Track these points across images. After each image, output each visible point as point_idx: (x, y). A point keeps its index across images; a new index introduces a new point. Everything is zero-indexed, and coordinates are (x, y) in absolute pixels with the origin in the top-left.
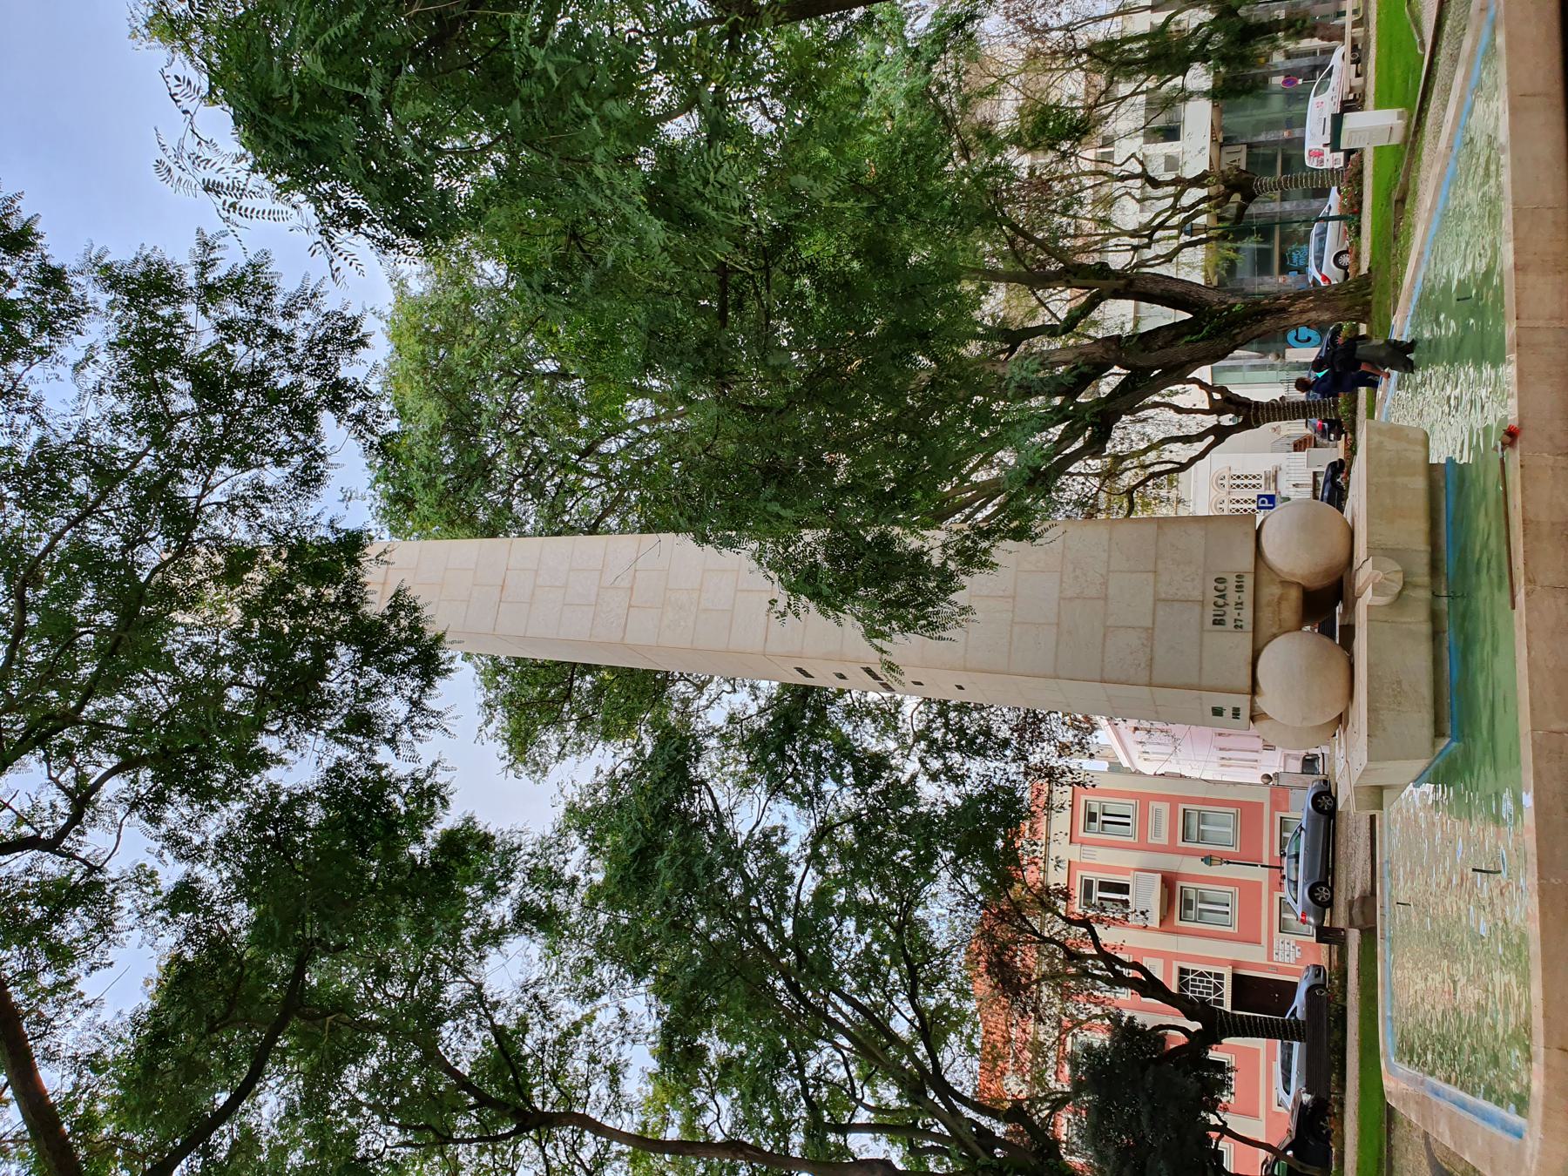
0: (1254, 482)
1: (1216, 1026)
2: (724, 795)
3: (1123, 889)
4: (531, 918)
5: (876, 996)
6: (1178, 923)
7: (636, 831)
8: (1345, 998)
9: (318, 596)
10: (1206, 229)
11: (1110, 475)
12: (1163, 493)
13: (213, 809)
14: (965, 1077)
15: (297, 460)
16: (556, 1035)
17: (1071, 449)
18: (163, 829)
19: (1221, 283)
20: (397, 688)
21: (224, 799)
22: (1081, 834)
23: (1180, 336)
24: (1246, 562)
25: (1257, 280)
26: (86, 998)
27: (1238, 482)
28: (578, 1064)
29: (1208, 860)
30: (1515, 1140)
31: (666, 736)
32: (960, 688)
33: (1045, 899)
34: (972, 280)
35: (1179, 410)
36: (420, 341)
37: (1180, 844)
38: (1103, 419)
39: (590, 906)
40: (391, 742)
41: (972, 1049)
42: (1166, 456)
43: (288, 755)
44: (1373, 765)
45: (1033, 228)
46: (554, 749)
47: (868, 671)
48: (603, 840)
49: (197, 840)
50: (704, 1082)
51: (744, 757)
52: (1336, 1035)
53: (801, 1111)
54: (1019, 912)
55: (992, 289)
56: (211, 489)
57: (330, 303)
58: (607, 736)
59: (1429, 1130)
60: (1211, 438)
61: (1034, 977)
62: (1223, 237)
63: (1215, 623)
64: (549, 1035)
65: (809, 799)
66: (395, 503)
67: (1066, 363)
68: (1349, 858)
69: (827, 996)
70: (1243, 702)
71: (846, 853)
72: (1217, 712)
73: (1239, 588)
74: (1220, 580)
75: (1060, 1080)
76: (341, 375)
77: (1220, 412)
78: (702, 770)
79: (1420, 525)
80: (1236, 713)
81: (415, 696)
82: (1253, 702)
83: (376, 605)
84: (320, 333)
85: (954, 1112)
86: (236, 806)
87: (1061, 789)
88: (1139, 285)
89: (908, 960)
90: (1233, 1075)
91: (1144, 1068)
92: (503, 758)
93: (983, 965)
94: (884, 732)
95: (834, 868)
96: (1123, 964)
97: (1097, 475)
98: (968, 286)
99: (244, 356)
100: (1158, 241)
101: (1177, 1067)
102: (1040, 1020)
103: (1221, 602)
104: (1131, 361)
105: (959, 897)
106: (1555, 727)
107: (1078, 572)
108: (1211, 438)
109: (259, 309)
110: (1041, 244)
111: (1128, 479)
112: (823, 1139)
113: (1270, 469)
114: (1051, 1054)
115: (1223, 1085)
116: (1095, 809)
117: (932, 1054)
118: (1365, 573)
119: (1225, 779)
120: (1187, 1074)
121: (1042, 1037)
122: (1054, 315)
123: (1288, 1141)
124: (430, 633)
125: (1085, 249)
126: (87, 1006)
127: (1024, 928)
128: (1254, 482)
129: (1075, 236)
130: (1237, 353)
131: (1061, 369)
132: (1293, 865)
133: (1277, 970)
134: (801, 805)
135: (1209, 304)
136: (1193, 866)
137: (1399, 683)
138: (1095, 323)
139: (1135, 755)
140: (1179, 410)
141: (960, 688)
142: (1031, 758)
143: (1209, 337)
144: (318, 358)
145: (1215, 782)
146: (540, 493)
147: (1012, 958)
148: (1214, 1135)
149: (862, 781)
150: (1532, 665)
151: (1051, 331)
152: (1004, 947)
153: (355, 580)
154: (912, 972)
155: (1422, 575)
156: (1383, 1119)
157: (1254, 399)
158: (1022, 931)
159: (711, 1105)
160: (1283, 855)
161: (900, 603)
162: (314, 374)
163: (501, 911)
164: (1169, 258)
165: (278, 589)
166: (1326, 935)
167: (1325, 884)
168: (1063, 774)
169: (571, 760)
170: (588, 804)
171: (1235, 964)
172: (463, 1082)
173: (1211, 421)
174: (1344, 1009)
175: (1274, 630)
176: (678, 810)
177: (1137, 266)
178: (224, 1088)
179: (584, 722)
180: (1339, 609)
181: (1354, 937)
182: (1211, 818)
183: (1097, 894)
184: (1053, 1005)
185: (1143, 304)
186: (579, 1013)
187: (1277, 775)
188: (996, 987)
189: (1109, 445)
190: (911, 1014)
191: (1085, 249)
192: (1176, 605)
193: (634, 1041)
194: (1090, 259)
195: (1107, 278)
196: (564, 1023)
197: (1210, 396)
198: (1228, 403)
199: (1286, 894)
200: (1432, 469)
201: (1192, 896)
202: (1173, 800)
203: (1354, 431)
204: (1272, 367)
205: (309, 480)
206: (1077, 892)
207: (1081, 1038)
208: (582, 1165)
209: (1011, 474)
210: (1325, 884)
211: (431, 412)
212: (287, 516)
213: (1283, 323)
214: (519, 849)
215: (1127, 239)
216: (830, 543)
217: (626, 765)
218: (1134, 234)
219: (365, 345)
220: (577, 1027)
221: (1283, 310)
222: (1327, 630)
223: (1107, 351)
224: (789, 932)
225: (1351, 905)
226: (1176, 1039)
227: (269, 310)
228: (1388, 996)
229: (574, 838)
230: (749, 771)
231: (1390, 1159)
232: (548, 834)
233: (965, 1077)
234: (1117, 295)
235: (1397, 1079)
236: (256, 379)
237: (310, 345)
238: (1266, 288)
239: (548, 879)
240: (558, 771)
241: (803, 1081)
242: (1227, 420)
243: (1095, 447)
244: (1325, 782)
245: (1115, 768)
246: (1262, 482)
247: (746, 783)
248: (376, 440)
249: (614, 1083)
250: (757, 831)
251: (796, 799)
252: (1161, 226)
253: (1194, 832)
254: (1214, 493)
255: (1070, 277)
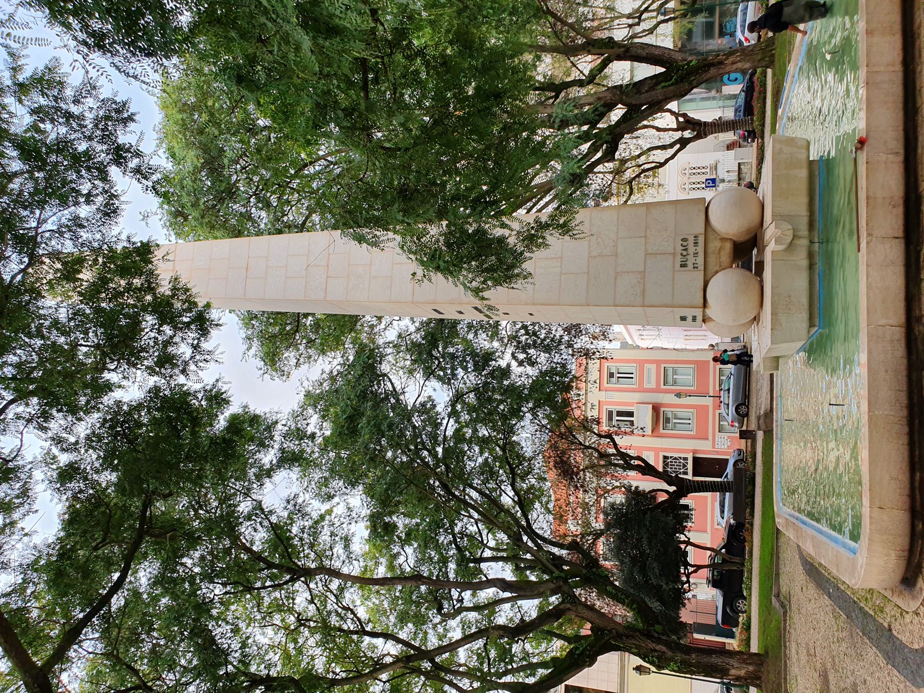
0: (703, 171)
1: (685, 488)
2: (398, 379)
3: (631, 414)
4: (288, 459)
5: (492, 485)
6: (662, 431)
7: (347, 405)
8: (754, 468)
9: (130, 284)
10: (674, 11)
11: (618, 172)
12: (650, 180)
13: (80, 419)
14: (545, 526)
15: (100, 200)
16: (310, 522)
17: (593, 160)
18: (50, 434)
19: (683, 46)
20: (183, 339)
21: (87, 412)
22: (606, 385)
23: (657, 84)
24: (700, 228)
25: (705, 42)
26: (26, 531)
27: (694, 171)
28: (325, 537)
29: (679, 395)
30: (851, 555)
31: (361, 349)
32: (531, 314)
33: (586, 425)
34: (530, 53)
35: (658, 129)
36: (181, 111)
37: (662, 387)
38: (614, 136)
39: (324, 449)
40: (183, 372)
41: (547, 509)
42: (651, 159)
43: (125, 383)
44: (774, 346)
45: (566, 16)
46: (293, 362)
47: (476, 308)
48: (329, 410)
49: (72, 439)
50: (397, 540)
51: (408, 357)
52: (750, 488)
53: (453, 552)
54: (571, 433)
55: (543, 57)
56: (45, 221)
57: (105, 92)
58: (323, 352)
59: (801, 545)
60: (678, 146)
61: (581, 467)
62: (684, 15)
63: (682, 266)
64: (306, 523)
65: (446, 380)
66: (176, 217)
67: (589, 104)
68: (758, 391)
69: (464, 490)
70: (698, 313)
71: (471, 409)
72: (683, 319)
73: (696, 244)
74: (684, 240)
75: (598, 524)
76: (121, 141)
77: (683, 129)
78: (385, 367)
79: (804, 200)
80: (694, 319)
81: (196, 342)
82: (704, 313)
83: (165, 289)
84: (101, 113)
85: (539, 547)
86: (96, 415)
87: (593, 362)
88: (633, 51)
89: (508, 463)
90: (693, 512)
91: (645, 514)
92: (261, 369)
93: (552, 463)
94: (492, 338)
95: (465, 417)
96: (632, 458)
97: (611, 172)
98: (528, 57)
99: (54, 131)
100: (644, 20)
101: (662, 512)
102: (585, 491)
103: (685, 253)
104: (629, 100)
105: (537, 427)
106: (881, 323)
107: (600, 240)
108: (678, 146)
109: (56, 99)
110: (571, 26)
111: (629, 174)
112: (467, 566)
113: (713, 162)
114: (593, 508)
115: (687, 517)
116: (613, 370)
117: (525, 515)
118: (770, 232)
119: (688, 347)
120: (667, 515)
121: (587, 500)
122: (582, 72)
123: (723, 544)
124: (201, 303)
125: (598, 29)
126: (26, 535)
127: (574, 442)
128: (703, 171)
129: (593, 20)
130: (695, 90)
131: (587, 108)
132: (726, 395)
133: (718, 453)
134: (444, 383)
135: (676, 61)
136: (670, 399)
137: (789, 296)
138: (606, 77)
139: (636, 338)
140: (658, 129)
141: (531, 314)
142: (575, 346)
143: (677, 82)
144: (103, 130)
145: (682, 350)
146: (267, 205)
147: (568, 458)
148: (683, 546)
149: (478, 368)
150: (869, 287)
151: (580, 83)
152: (564, 453)
153: (151, 273)
154: (512, 471)
155: (804, 230)
156: (774, 535)
157: (703, 120)
158: (573, 443)
159: (403, 553)
160: (721, 390)
161: (491, 270)
162: (101, 142)
163: (268, 458)
164: (651, 31)
165: (102, 282)
166: (744, 435)
167: (744, 404)
168: (594, 353)
169: (304, 368)
170: (318, 391)
171: (694, 452)
172: (257, 557)
173: (678, 135)
174: (754, 474)
175: (717, 268)
176: (372, 392)
177: (632, 37)
178: (116, 571)
179: (311, 342)
180: (755, 252)
181: (760, 435)
182: (679, 371)
183: (615, 418)
184: (593, 482)
185: (636, 64)
186: (326, 507)
187: (717, 344)
188: (560, 475)
189: (617, 153)
190: (511, 493)
191: (598, 29)
192: (658, 257)
193: (356, 522)
194: (604, 35)
195: (612, 48)
196: (315, 515)
197: (677, 119)
198: (688, 123)
199: (723, 410)
200: (811, 163)
201: (670, 415)
202: (658, 363)
203: (763, 138)
204: (714, 98)
205: (110, 212)
206: (604, 419)
207: (609, 500)
208: (331, 592)
209: (560, 178)
210: (744, 404)
211: (192, 158)
212: (98, 236)
213: (721, 71)
214: (276, 422)
215: (625, 20)
216: (448, 235)
217: (339, 367)
218: (629, 16)
219: (133, 120)
220: (322, 517)
221: (721, 63)
222: (747, 266)
223: (614, 95)
224: (440, 455)
225: (759, 418)
226: (662, 497)
227: (64, 100)
228: (778, 470)
229: (310, 411)
230: (412, 364)
231: (778, 553)
232: (296, 409)
233: (545, 526)
234: (620, 58)
235: (783, 511)
236: (62, 146)
237: (97, 122)
238: (710, 48)
239: (299, 434)
240: (296, 374)
241: (454, 536)
242: (687, 134)
243: (609, 156)
244: (744, 346)
245: (624, 345)
246: (708, 170)
247: (411, 372)
248: (150, 184)
249: (347, 547)
250: (418, 402)
251: (440, 379)
252: (646, 10)
253: (670, 380)
254: (680, 179)
255: (590, 48)
